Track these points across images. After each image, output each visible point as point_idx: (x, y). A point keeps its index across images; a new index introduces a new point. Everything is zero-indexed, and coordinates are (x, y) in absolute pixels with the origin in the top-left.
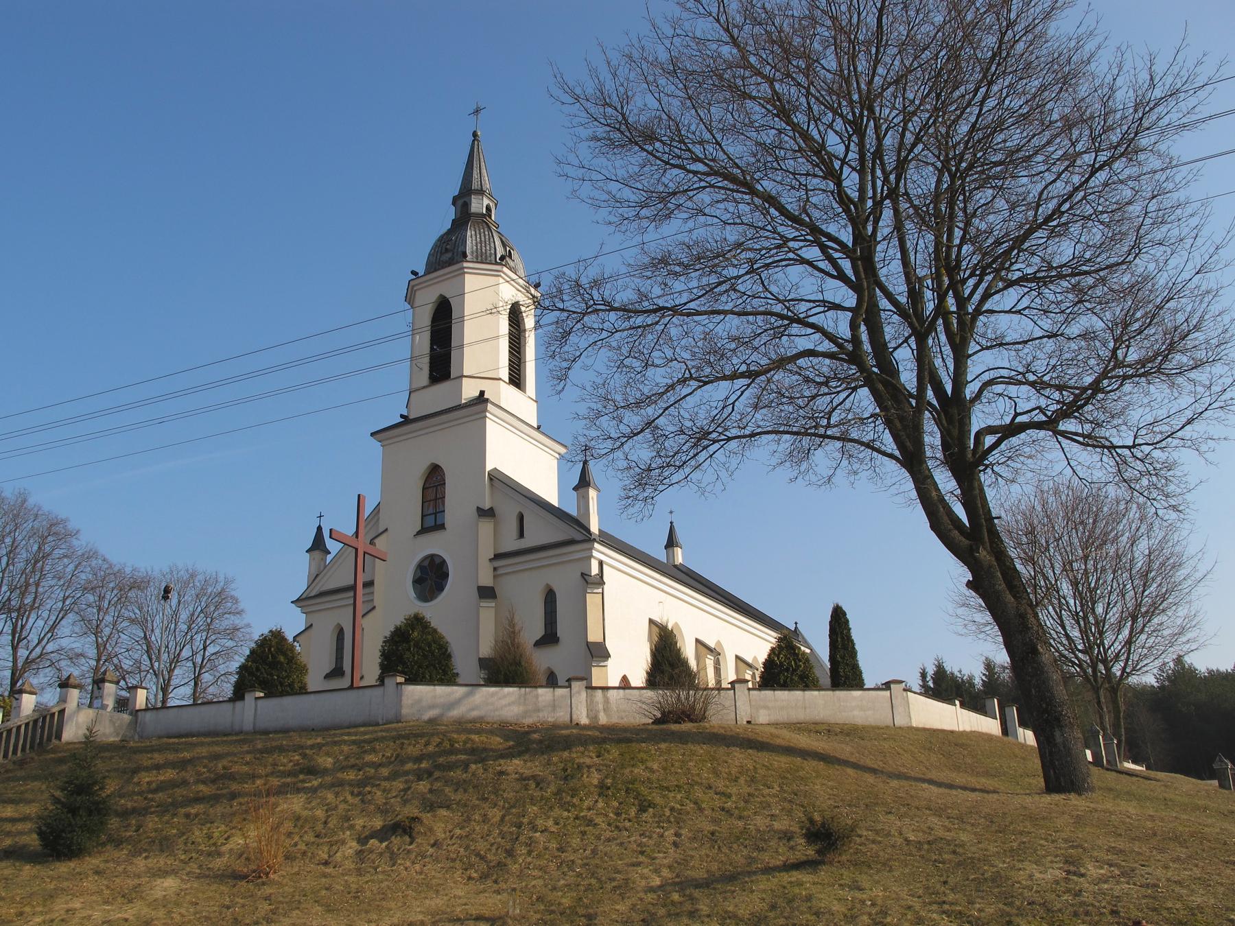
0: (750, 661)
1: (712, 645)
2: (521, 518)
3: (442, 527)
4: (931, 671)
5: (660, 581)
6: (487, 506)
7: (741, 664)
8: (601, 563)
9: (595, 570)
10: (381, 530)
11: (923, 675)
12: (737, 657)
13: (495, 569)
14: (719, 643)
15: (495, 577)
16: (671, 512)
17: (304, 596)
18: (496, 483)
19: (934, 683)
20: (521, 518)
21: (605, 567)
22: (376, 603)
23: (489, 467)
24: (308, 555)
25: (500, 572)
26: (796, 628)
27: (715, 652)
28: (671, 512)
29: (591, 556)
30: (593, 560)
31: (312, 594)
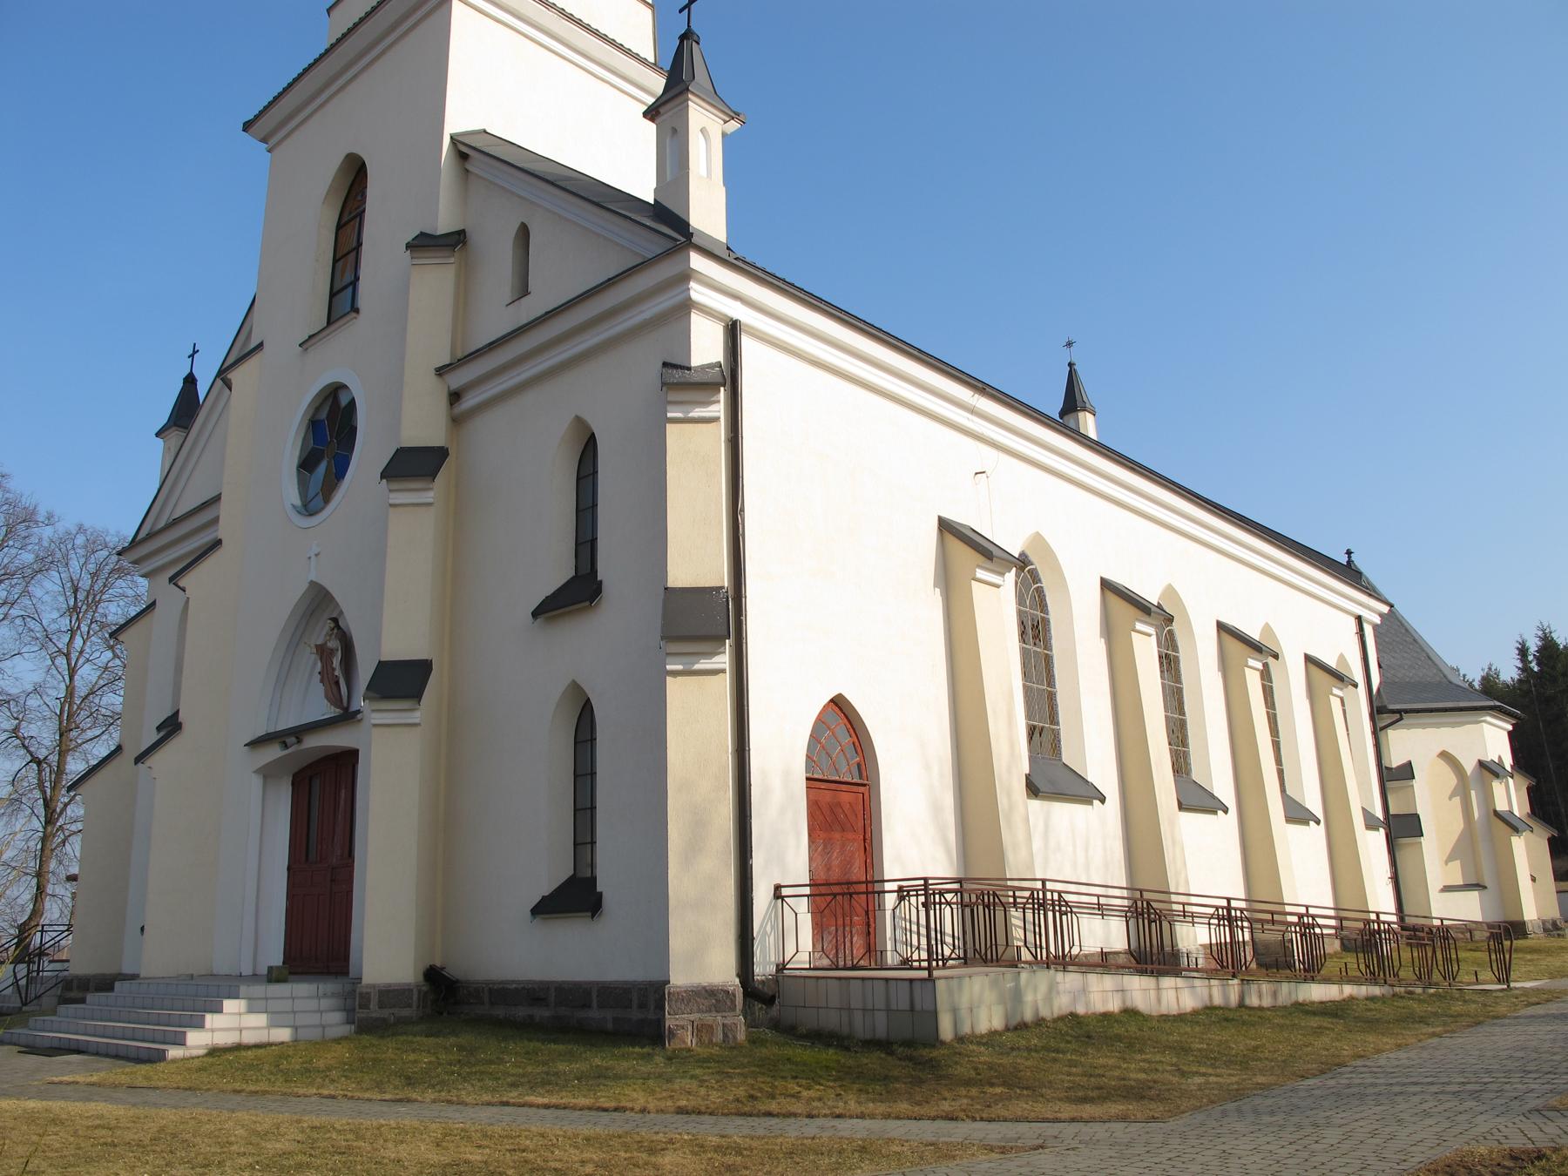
0: (1255, 634)
1: (1152, 596)
2: (524, 233)
3: (357, 311)
4: (1533, 645)
5: (973, 411)
6: (444, 223)
7: (1234, 646)
8: (733, 331)
9: (706, 346)
10: (253, 345)
11: (1523, 651)
12: (1222, 627)
13: (455, 397)
14: (1170, 591)
15: (457, 421)
16: (1069, 344)
17: (142, 535)
18: (476, 165)
19: (1538, 664)
20: (524, 233)
21: (746, 343)
22: (222, 531)
23: (460, 117)
24: (160, 441)
25: (468, 402)
26: (1350, 562)
27: (1161, 617)
28: (1069, 344)
29: (686, 306)
30: (697, 322)
31: (162, 524)
